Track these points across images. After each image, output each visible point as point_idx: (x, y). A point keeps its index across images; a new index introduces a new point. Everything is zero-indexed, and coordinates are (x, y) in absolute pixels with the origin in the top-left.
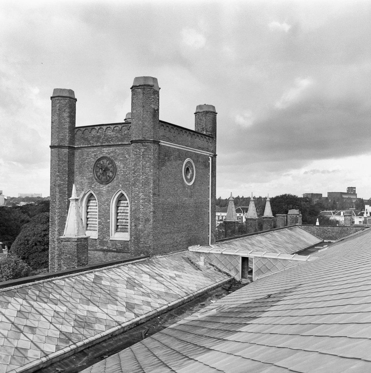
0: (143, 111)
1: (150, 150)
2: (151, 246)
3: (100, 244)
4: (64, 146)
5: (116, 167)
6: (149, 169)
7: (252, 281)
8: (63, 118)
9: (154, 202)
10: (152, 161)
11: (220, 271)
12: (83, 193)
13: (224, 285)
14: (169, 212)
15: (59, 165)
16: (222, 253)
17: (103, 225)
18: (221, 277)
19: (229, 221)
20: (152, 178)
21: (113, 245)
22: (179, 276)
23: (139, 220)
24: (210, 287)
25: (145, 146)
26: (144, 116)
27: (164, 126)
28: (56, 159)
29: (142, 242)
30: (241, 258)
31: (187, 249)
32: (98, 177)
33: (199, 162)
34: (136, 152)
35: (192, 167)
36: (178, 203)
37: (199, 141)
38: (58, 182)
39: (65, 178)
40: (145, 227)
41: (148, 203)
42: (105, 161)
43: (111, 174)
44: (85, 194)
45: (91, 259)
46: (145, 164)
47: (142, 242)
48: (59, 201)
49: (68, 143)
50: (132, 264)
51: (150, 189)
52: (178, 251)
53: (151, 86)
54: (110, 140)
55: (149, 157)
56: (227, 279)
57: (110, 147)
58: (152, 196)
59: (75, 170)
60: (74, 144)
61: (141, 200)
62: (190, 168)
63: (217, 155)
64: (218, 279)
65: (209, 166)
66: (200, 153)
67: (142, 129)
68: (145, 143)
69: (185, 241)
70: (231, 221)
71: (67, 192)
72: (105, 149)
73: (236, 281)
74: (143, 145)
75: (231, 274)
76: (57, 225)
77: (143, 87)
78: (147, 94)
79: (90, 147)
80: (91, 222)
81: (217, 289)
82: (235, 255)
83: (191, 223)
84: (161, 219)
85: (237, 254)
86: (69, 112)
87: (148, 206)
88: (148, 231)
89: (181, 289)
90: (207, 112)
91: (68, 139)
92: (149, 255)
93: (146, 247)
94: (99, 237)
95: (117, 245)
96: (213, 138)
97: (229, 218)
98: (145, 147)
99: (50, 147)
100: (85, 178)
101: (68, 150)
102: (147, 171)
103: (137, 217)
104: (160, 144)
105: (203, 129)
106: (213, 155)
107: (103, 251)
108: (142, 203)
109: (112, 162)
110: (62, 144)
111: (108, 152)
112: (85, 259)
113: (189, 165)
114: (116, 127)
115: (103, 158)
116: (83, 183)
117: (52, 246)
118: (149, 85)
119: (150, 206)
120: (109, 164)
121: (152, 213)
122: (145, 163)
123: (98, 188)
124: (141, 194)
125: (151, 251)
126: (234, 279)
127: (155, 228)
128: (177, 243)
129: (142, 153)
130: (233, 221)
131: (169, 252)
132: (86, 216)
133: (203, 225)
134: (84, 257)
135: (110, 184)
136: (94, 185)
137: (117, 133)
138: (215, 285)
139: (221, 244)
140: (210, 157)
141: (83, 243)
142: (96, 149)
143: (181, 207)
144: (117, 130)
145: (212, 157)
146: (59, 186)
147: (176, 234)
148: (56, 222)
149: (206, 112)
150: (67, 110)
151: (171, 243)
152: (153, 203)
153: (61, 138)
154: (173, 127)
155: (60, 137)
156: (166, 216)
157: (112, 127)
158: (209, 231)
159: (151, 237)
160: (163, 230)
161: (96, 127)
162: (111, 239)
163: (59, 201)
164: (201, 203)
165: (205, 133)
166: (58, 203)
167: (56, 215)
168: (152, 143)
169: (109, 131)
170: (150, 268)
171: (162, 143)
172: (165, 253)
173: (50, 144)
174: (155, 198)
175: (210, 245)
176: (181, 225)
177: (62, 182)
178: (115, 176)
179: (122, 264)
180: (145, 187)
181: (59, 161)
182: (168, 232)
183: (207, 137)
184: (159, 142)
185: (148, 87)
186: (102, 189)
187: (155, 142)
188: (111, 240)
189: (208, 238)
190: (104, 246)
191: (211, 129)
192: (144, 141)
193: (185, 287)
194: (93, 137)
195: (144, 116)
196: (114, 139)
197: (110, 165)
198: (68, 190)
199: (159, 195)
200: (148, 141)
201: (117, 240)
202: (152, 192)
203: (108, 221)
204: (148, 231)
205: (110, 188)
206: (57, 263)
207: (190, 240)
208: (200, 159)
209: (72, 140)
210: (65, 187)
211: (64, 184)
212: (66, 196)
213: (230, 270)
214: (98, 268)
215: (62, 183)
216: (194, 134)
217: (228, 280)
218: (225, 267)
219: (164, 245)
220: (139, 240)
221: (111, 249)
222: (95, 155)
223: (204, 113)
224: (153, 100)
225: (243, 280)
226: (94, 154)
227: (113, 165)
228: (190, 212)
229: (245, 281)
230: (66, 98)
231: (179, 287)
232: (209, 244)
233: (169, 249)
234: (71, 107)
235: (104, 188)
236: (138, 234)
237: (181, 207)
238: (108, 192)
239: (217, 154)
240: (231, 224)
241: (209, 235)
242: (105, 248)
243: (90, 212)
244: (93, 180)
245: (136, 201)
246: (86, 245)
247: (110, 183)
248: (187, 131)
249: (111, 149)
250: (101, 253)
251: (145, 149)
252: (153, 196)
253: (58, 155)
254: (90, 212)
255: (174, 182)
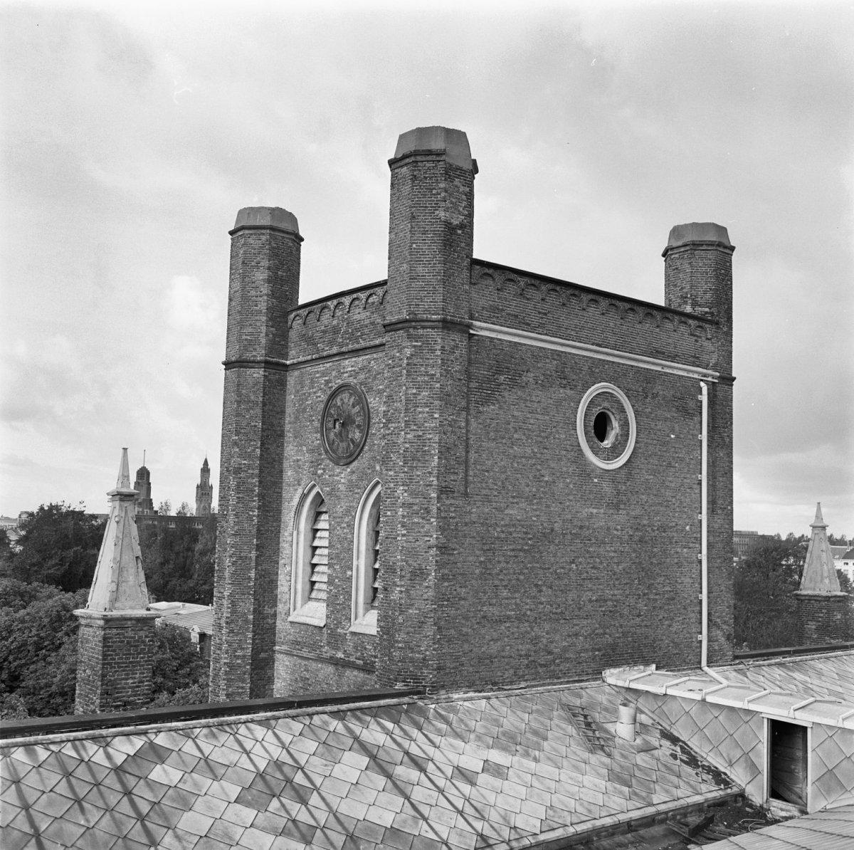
0: (410, 231)
1: (433, 351)
2: (428, 661)
3: (329, 643)
4: (253, 362)
5: (369, 414)
6: (427, 409)
7: (804, 812)
8: (253, 285)
9: (443, 515)
10: (438, 385)
11: (693, 761)
12: (300, 491)
13: (685, 815)
14: (513, 550)
15: (238, 415)
16: (704, 700)
17: (337, 587)
18: (682, 784)
19: (810, 592)
20: (437, 439)
21: (355, 647)
22: (497, 771)
23: (394, 572)
24: (608, 821)
25: (417, 338)
26: (414, 246)
27: (494, 279)
28: (233, 396)
29: (400, 645)
30: (765, 721)
31: (597, 674)
32: (331, 444)
33: (653, 398)
34: (393, 358)
35: (623, 410)
36: (556, 525)
37: (680, 337)
38: (235, 461)
39: (254, 450)
40: (409, 597)
41: (423, 518)
42: (345, 396)
43: (358, 434)
44: (304, 497)
45: (310, 685)
46: (414, 394)
47: (400, 645)
48: (235, 515)
49: (263, 352)
50: (332, 714)
51: (430, 473)
52: (555, 681)
53: (438, 155)
54: (359, 334)
55: (427, 374)
56: (711, 792)
57: (358, 356)
58: (434, 495)
59: (287, 427)
60: (286, 356)
61: (401, 509)
62: (613, 414)
63: (735, 378)
64: (667, 791)
65: (701, 413)
66: (659, 369)
67: (408, 287)
68: (415, 328)
69: (587, 650)
70: (817, 593)
71: (256, 488)
72: (347, 362)
73: (751, 806)
74: (410, 337)
75: (732, 777)
76: (228, 581)
77: (413, 159)
78: (426, 178)
79: (316, 359)
80: (319, 575)
81: (642, 832)
82: (748, 712)
83: (616, 592)
84: (477, 571)
85: (752, 707)
86: (269, 268)
87: (423, 527)
88: (420, 609)
89: (470, 819)
90: (695, 245)
91: (263, 341)
92: (421, 689)
93: (412, 660)
94: (329, 621)
95: (365, 649)
96: (717, 323)
97: (812, 585)
98: (417, 341)
99: (224, 363)
100: (305, 448)
101: (265, 371)
102: (420, 416)
103: (391, 564)
104: (471, 332)
105: (684, 298)
106: (719, 378)
107: (334, 662)
108: (403, 516)
109: (361, 401)
110: (248, 356)
111: (354, 371)
112: (138, 687)
113: (606, 404)
114: (371, 295)
115: (343, 389)
116: (300, 463)
117: (217, 639)
118: (429, 153)
119: (427, 527)
120: (354, 406)
121: (433, 551)
122: (414, 391)
123: (330, 476)
124: (401, 488)
125: (429, 676)
126: (742, 795)
127: (442, 599)
128: (550, 653)
129: (405, 362)
130: (824, 593)
131: (511, 683)
132: (310, 558)
133: (674, 599)
134: (130, 681)
135: (355, 464)
136: (323, 469)
137: (373, 313)
138: (635, 815)
139: (760, 666)
140: (702, 384)
141: (131, 634)
142: (328, 365)
143: (569, 537)
144: (373, 303)
145: (714, 383)
146: (238, 471)
147: (547, 626)
148: (227, 574)
149: (694, 245)
150: (265, 263)
151: (523, 653)
152: (437, 518)
153: (246, 340)
154: (537, 282)
155: (244, 337)
156: (499, 562)
157: (363, 295)
158: (701, 623)
159: (430, 630)
160: (485, 609)
161: (329, 303)
162: (353, 629)
163: (235, 515)
164: (663, 528)
165: (688, 309)
166: (231, 518)
167: (227, 554)
168: (438, 328)
169: (357, 311)
170: (397, 731)
171: (482, 329)
172: (494, 684)
173: (224, 359)
174: (448, 502)
175: (706, 669)
176: (571, 595)
177: (245, 462)
178: (366, 440)
179: (289, 712)
180: (412, 468)
181: (239, 402)
182: (509, 617)
183: (690, 321)
184: (470, 326)
185: (429, 158)
186: (338, 478)
187: (449, 325)
188: (354, 634)
189: (695, 644)
190: (337, 649)
191: (708, 296)
192: (413, 324)
193: (494, 816)
194: (324, 332)
195: (414, 246)
196: (366, 331)
197: (357, 408)
198: (260, 482)
199: (466, 495)
200: (426, 324)
201: (366, 635)
202: (435, 483)
203: (349, 573)
204: (420, 609)
205: (354, 477)
206: (224, 689)
207: (614, 647)
208: (658, 388)
209: (279, 342)
210: (252, 476)
211: (249, 467)
212: (254, 501)
213: (731, 762)
214: (178, 721)
215: (244, 464)
216: (632, 309)
217: (706, 800)
218: (715, 748)
219: (491, 657)
220: (393, 636)
221: (352, 659)
222: (327, 382)
223: (688, 248)
224: (443, 194)
225: (776, 804)
226: (325, 381)
227: (363, 408)
228: (612, 554)
229: (782, 810)
230: (263, 231)
231: (469, 810)
232: (700, 662)
233: (512, 671)
234: (277, 255)
235: (343, 476)
236: (390, 617)
237: (569, 537)
238: (351, 486)
239: (734, 375)
240: (816, 605)
241: (701, 633)
242: (340, 655)
243: (321, 547)
244: (320, 454)
245: (389, 513)
246: (143, 642)
247: (354, 460)
248: (601, 299)
249: (361, 360)
250: (330, 669)
251: (415, 346)
252: (439, 498)
253: (238, 385)
254: (321, 547)
255: (539, 456)
